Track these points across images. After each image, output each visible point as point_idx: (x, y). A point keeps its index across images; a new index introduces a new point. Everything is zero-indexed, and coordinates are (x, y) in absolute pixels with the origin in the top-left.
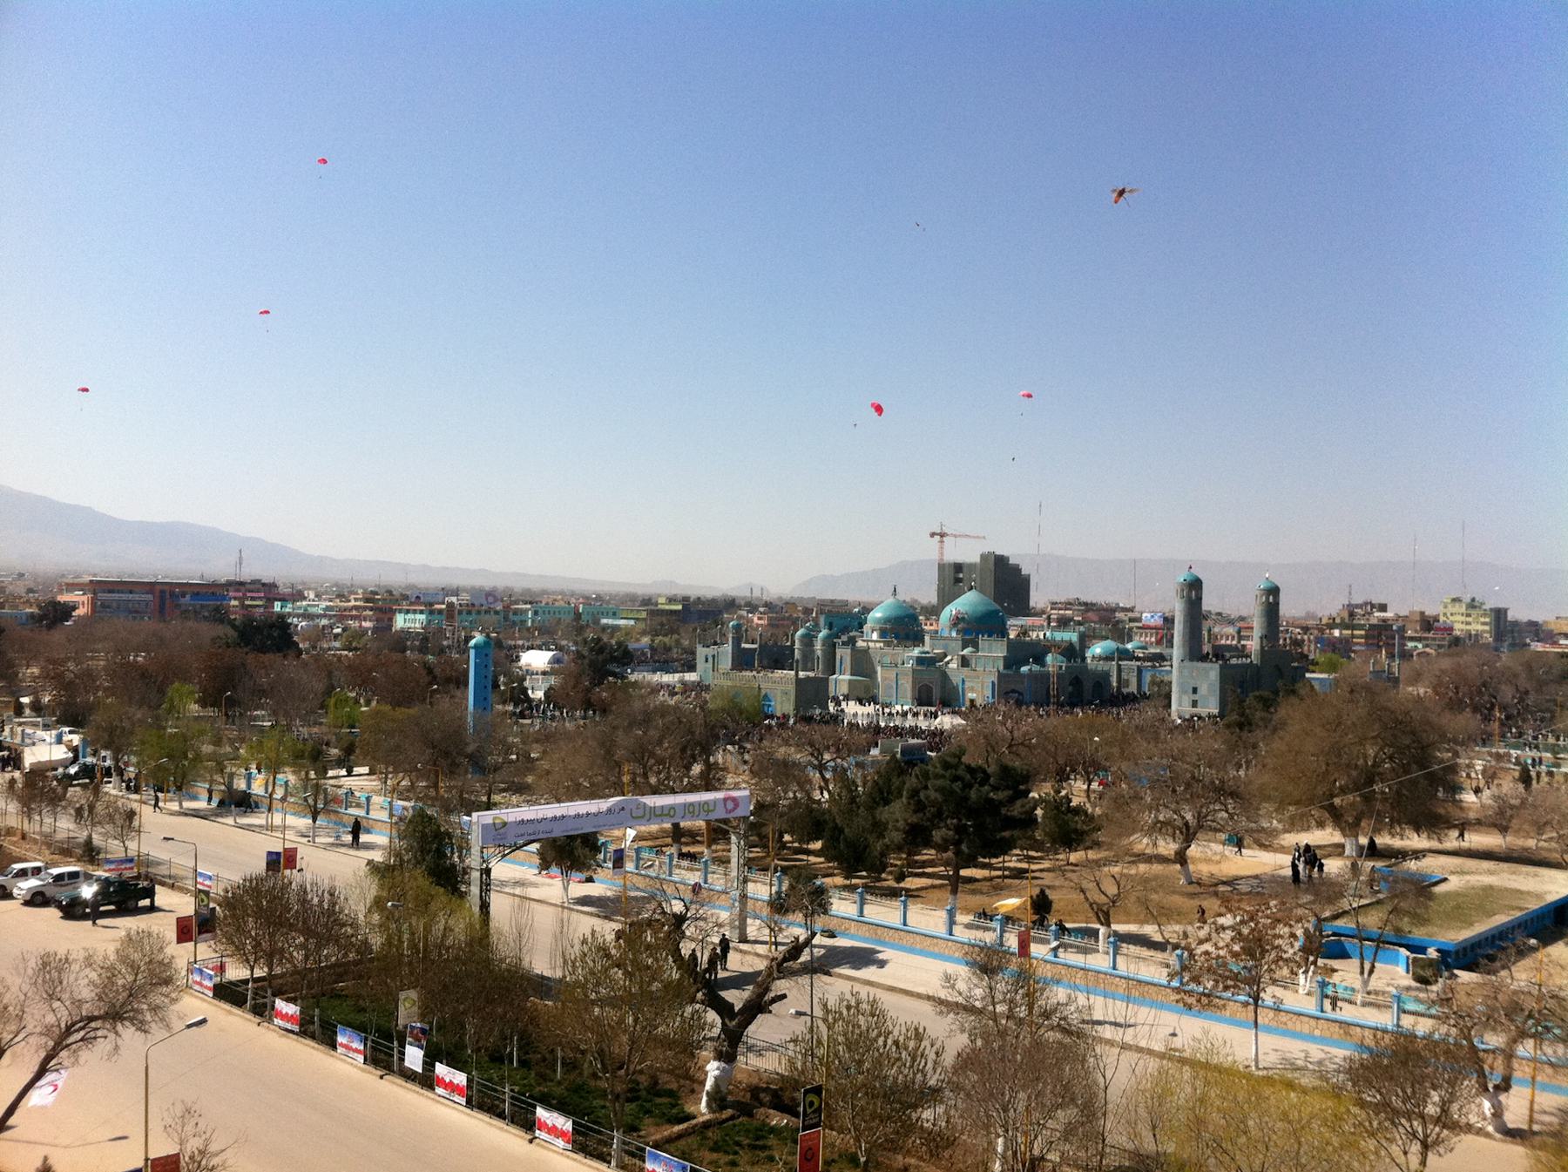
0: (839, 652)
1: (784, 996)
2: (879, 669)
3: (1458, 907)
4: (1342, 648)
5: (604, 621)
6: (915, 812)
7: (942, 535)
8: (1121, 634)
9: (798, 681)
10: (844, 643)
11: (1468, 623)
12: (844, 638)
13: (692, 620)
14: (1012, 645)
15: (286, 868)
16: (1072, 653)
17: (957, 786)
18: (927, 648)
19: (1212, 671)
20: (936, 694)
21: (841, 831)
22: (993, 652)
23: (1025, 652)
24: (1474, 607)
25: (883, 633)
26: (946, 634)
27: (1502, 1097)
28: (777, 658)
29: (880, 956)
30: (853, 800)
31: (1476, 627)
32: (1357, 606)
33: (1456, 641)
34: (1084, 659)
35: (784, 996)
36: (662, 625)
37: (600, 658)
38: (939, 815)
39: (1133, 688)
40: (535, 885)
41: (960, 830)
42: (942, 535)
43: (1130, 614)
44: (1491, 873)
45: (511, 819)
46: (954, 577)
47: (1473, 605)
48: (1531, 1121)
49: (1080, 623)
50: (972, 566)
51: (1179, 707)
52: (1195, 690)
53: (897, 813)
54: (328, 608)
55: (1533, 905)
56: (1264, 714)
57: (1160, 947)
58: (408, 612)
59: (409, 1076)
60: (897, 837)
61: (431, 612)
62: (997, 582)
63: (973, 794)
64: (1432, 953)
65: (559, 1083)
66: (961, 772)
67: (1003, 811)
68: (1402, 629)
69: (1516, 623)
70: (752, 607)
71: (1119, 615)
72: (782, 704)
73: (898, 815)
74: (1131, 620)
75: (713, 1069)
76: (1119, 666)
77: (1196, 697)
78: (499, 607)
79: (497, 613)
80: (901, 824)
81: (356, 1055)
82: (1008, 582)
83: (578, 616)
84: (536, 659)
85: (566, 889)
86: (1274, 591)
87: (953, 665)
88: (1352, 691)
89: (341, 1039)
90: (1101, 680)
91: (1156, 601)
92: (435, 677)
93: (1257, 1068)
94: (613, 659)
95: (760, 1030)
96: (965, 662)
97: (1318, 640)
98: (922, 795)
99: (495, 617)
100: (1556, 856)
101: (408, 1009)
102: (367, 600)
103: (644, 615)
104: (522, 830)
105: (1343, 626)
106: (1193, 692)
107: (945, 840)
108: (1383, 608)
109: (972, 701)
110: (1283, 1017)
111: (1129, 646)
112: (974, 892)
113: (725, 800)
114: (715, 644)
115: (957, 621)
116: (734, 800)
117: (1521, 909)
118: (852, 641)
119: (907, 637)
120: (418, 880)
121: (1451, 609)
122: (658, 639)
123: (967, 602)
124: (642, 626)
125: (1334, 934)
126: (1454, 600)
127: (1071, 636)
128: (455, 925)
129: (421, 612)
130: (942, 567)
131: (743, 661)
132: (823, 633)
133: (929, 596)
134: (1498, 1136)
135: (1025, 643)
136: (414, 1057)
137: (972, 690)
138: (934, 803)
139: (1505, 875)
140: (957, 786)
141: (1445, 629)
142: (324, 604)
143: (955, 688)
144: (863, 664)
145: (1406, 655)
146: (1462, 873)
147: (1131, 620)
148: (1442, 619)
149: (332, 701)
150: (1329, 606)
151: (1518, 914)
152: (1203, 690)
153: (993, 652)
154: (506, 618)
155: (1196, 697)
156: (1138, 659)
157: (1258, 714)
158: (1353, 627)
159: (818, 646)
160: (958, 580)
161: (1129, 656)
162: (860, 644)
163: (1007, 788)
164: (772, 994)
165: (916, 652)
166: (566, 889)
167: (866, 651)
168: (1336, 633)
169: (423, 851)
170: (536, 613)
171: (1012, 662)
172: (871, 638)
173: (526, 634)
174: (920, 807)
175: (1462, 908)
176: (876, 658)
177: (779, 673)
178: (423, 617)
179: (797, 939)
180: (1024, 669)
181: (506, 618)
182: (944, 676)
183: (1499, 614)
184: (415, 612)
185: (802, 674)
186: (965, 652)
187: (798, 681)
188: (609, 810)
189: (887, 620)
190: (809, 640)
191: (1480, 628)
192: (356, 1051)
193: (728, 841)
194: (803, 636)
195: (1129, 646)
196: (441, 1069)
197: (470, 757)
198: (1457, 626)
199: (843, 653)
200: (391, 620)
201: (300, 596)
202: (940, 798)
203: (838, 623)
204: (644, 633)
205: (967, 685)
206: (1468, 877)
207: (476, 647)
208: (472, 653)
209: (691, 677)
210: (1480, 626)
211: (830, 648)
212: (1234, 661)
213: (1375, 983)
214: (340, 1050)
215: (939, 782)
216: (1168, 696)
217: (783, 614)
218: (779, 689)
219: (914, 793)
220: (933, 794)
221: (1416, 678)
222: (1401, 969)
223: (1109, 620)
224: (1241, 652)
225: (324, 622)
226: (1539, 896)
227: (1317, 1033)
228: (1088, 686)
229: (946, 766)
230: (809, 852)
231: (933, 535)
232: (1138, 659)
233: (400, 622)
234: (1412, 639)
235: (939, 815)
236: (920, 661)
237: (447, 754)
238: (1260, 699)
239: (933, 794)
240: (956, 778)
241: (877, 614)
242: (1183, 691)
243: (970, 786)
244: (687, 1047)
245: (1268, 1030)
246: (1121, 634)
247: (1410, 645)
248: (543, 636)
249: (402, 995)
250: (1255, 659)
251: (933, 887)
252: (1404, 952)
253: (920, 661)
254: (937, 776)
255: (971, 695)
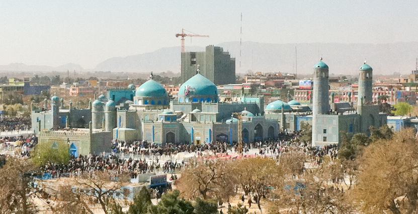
0: (119, 113)
2: (143, 123)
7: (183, 36)
8: (286, 92)
9: (93, 136)
10: (122, 108)
12: (122, 105)
14: (222, 107)
16: (256, 109)
18: (171, 110)
22: (210, 111)
23: (226, 112)
25: (145, 102)
26: (182, 101)
28: (80, 120)
34: (263, 113)
36: (11, 97)
39: (291, 130)
42: (183, 36)
43: (293, 81)
46: (191, 61)
50: (201, 54)
51: (317, 141)
52: (325, 131)
56: (361, 147)
70: (69, 81)
71: (287, 82)
72: (83, 149)
74: (294, 84)
76: (284, 116)
77: (325, 135)
82: (223, 66)
87: (187, 120)
88: (404, 141)
90: (273, 126)
91: (305, 71)
96: (193, 118)
97: (398, 94)
106: (325, 131)
109: (198, 142)
111: (290, 103)
114: (43, 110)
115: (189, 94)
119: (159, 103)
122: (8, 107)
123: (196, 82)
127: (256, 100)
131: (59, 123)
132: (109, 102)
133: (175, 68)
135: (229, 105)
137: (198, 134)
144: (133, 121)
147: (294, 84)
152: (329, 131)
153: (210, 111)
155: (325, 135)
156: (295, 111)
157: (358, 147)
159: (106, 110)
160: (193, 63)
161: (287, 109)
162: (131, 108)
165: (165, 112)
167: (135, 113)
168: (408, 89)
171: (221, 117)
172: (137, 105)
176: (141, 117)
180: (228, 121)
182: (182, 127)
185: (94, 131)
186: (194, 111)
187: (93, 136)
189: (148, 94)
190: (100, 107)
193: (117, 108)
194: (97, 104)
195: (290, 103)
199: (121, 115)
203: (118, 96)
209: (26, 132)
211: (113, 111)
212: (346, 113)
217: (87, 84)
218: (80, 141)
223: (281, 85)
228: (265, 129)
231: (177, 35)
232: (295, 111)
238: (359, 137)
246: (286, 92)
250: (359, 112)
253: (167, 118)
255: (197, 138)
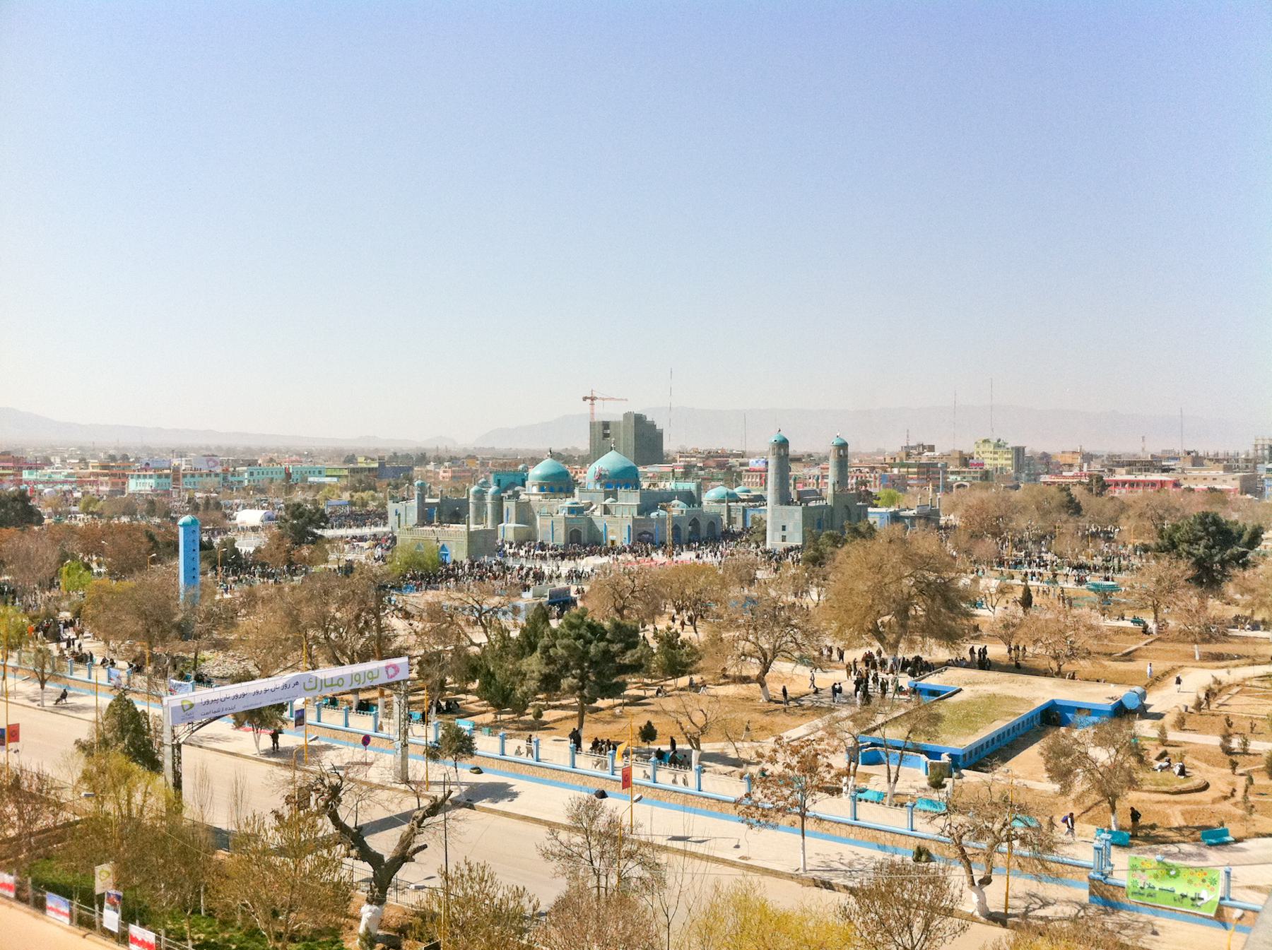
0: (506, 504)
1: (425, 847)
3: (968, 715)
4: (900, 484)
5: (311, 479)
6: (547, 664)
7: (593, 399)
11: (995, 459)
12: (510, 492)
13: (387, 474)
14: (645, 495)
15: (10, 741)
17: (579, 643)
18: (576, 500)
19: (796, 513)
20: (584, 538)
21: (493, 675)
22: (629, 500)
23: (651, 502)
24: (999, 446)
25: (541, 489)
26: (591, 488)
27: (986, 889)
28: (454, 513)
29: (515, 789)
30: (504, 647)
31: (1001, 462)
32: (913, 448)
33: (986, 476)
34: (700, 504)
35: (425, 847)
36: (360, 482)
37: (301, 521)
38: (566, 667)
39: (737, 527)
40: (226, 739)
41: (583, 678)
42: (593, 399)
43: (741, 460)
44: (995, 682)
45: (197, 701)
46: (603, 433)
47: (998, 445)
48: (1007, 907)
49: (701, 469)
50: (617, 424)
52: (784, 528)
53: (533, 664)
54: (69, 475)
55: (1025, 711)
57: (737, 763)
58: (139, 476)
59: (107, 933)
60: (533, 684)
61: (160, 476)
62: (638, 436)
63: (592, 649)
64: (945, 759)
65: (239, 929)
66: (583, 631)
67: (618, 660)
68: (946, 466)
69: (1031, 458)
70: (439, 461)
71: (732, 461)
73: (534, 667)
74: (742, 465)
75: (367, 911)
77: (784, 533)
78: (219, 470)
79: (217, 475)
80: (536, 675)
81: (62, 918)
82: (647, 440)
83: (289, 475)
84: (250, 517)
85: (257, 743)
86: (844, 446)
87: (597, 513)
89: (49, 904)
90: (714, 522)
92: (156, 543)
93: (805, 870)
94: (311, 522)
95: (406, 873)
96: (606, 510)
97: (882, 478)
98: (551, 652)
99: (217, 479)
100: (1042, 664)
101: (103, 879)
102: (104, 467)
103: (346, 473)
104: (207, 708)
105: (902, 465)
106: (784, 528)
107: (570, 687)
108: (931, 448)
109: (613, 542)
110: (826, 825)
111: (736, 490)
112: (597, 721)
113: (387, 667)
114: (404, 499)
115: (600, 477)
116: (395, 667)
117: (1015, 714)
118: (516, 495)
119: (561, 490)
120: (117, 759)
121: (982, 448)
122: (357, 495)
123: (610, 461)
124: (344, 482)
125: (873, 745)
126: (985, 441)
127: (690, 486)
128: (146, 796)
129: (151, 477)
130: (592, 425)
132: (493, 489)
133: (582, 444)
134: (982, 919)
136: (111, 919)
137: (613, 532)
138: (562, 657)
139: (1006, 684)
140: (579, 643)
141: (978, 465)
142: (66, 472)
143: (601, 534)
145: (948, 488)
146: (974, 683)
148: (976, 456)
149: (65, 569)
150: (893, 445)
151: (1013, 719)
152: (790, 528)
153: (629, 500)
154: (225, 479)
155: (784, 533)
156: (743, 501)
157: (829, 549)
158: (909, 466)
159: (489, 499)
160: (606, 436)
161: (733, 498)
162: (523, 497)
163: (621, 641)
164: (414, 846)
165: (568, 502)
166: (257, 743)
167: (528, 503)
168: (896, 471)
169: (123, 730)
170: (252, 474)
171: (644, 509)
172: (531, 493)
173: (243, 493)
174: (550, 661)
175: (968, 718)
176: (536, 509)
177: (454, 527)
178: (152, 482)
179: (436, 798)
180: (653, 515)
181: (225, 479)
183: (1019, 451)
184: (145, 476)
185: (473, 527)
186: (607, 502)
188: (285, 686)
189: (546, 477)
190: (480, 495)
191: (1004, 462)
192: (63, 913)
194: (476, 492)
195: (736, 490)
196: (135, 930)
197: (178, 627)
198: (987, 462)
199: (509, 505)
200: (124, 484)
201: (47, 462)
202: (566, 654)
204: (344, 489)
205: (609, 529)
206: (977, 687)
207: (184, 525)
208: (181, 530)
210: (1005, 461)
211: (499, 502)
212: (812, 504)
213: (900, 787)
214: (49, 913)
215: (565, 641)
216: (764, 532)
217: (463, 465)
218: (453, 541)
219: (546, 649)
220: (560, 651)
221: (953, 508)
222: (922, 772)
223: (724, 466)
224: (819, 495)
225: (66, 487)
226: (1030, 702)
227: (852, 836)
228: (703, 525)
229: (572, 626)
230: (467, 692)
231: (585, 399)
232: (743, 501)
233: (133, 486)
234: (952, 473)
235: (566, 667)
236: (571, 510)
237: (158, 622)
238: (830, 536)
239: (560, 651)
240: (579, 637)
241: (536, 472)
242: (774, 530)
243: (590, 642)
244: (342, 893)
245: (815, 835)
247: (952, 478)
248: (257, 494)
249: (98, 869)
250: (829, 502)
251: (567, 718)
252: (924, 758)
253: (571, 510)
254: (564, 636)
255: (611, 537)
